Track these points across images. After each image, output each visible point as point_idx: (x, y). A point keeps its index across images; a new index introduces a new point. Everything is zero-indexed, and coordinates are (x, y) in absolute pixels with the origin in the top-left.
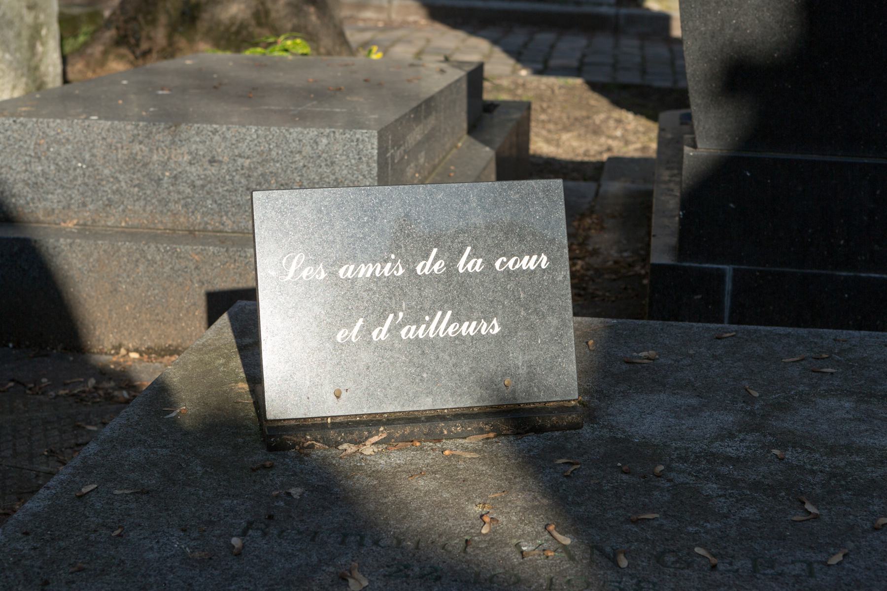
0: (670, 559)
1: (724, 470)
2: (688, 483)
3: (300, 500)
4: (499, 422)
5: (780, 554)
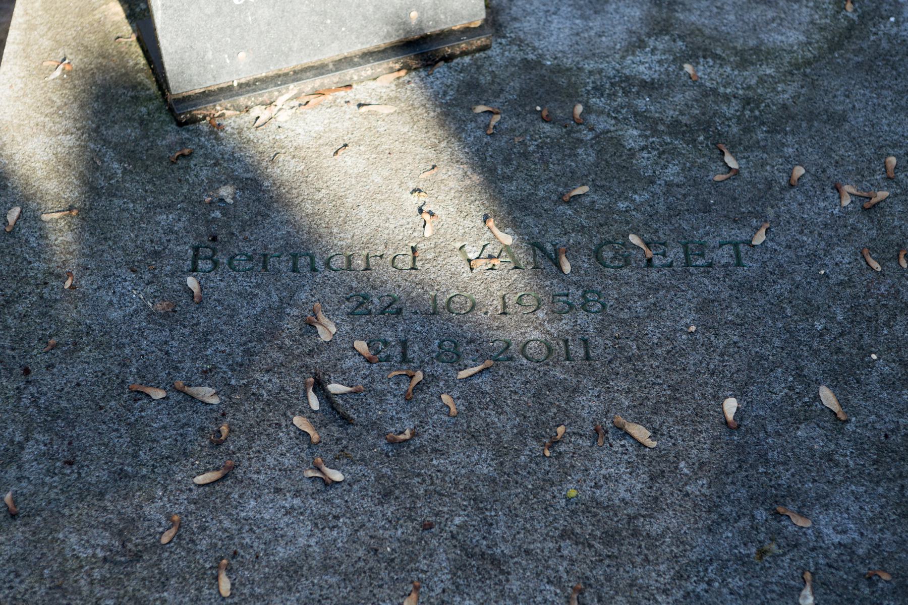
2: (609, 131)
3: (235, 205)
5: (708, 234)
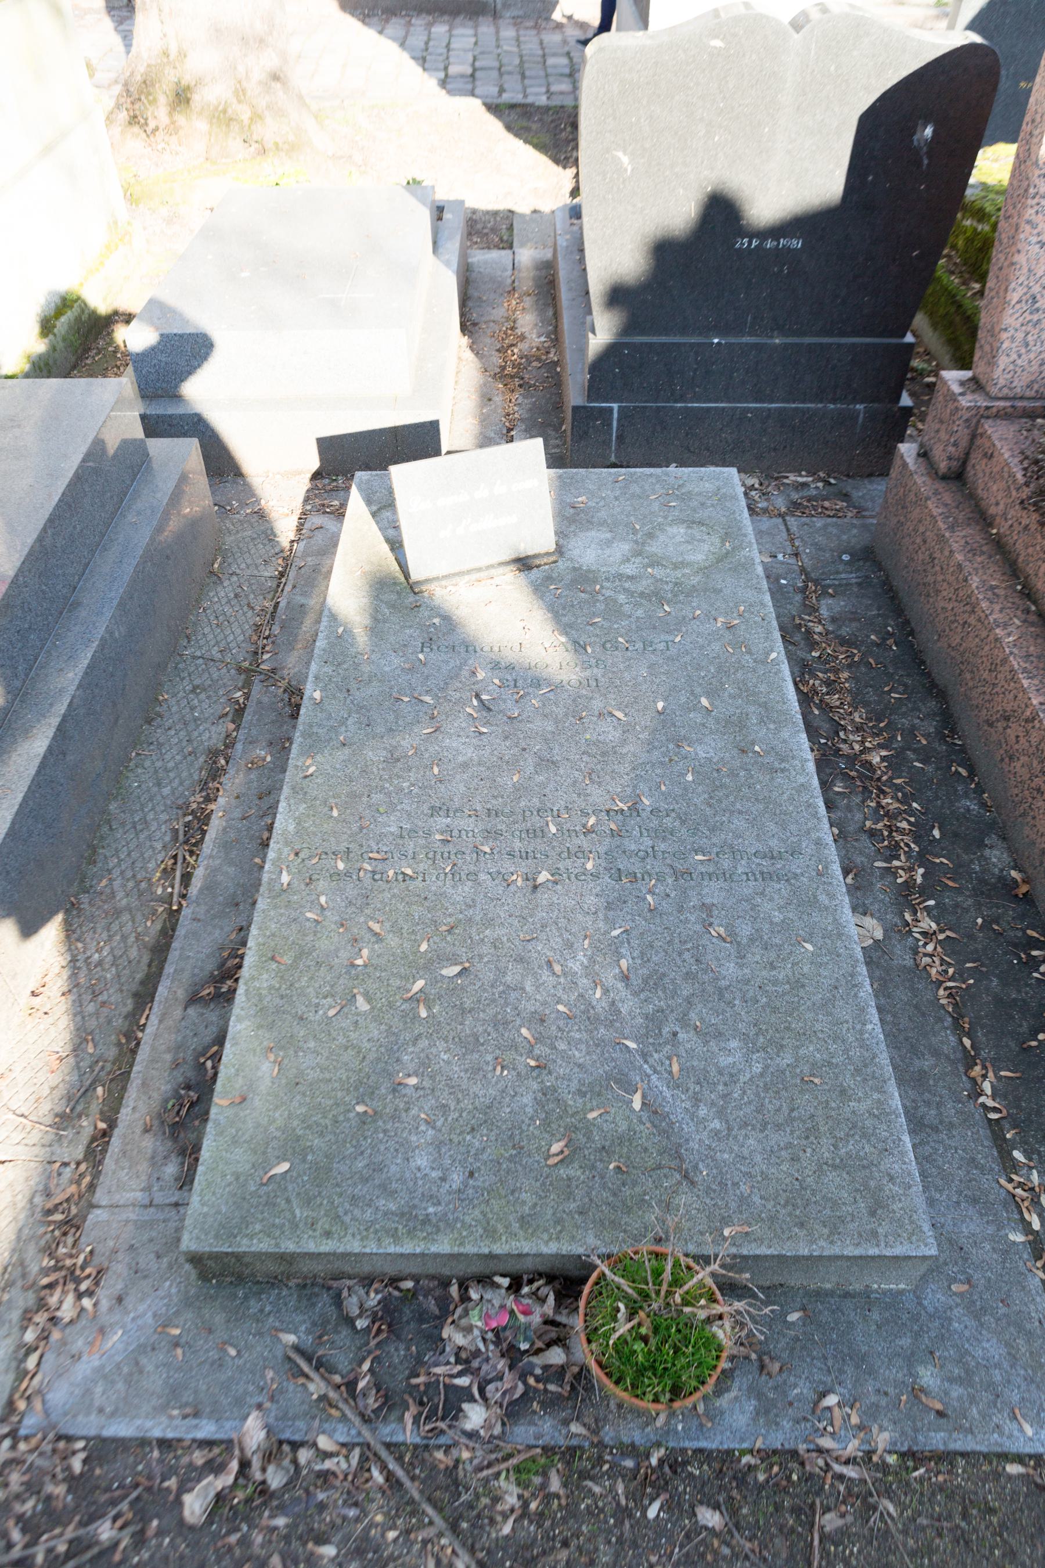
0: (608, 645)
1: (627, 585)
4: (517, 565)
